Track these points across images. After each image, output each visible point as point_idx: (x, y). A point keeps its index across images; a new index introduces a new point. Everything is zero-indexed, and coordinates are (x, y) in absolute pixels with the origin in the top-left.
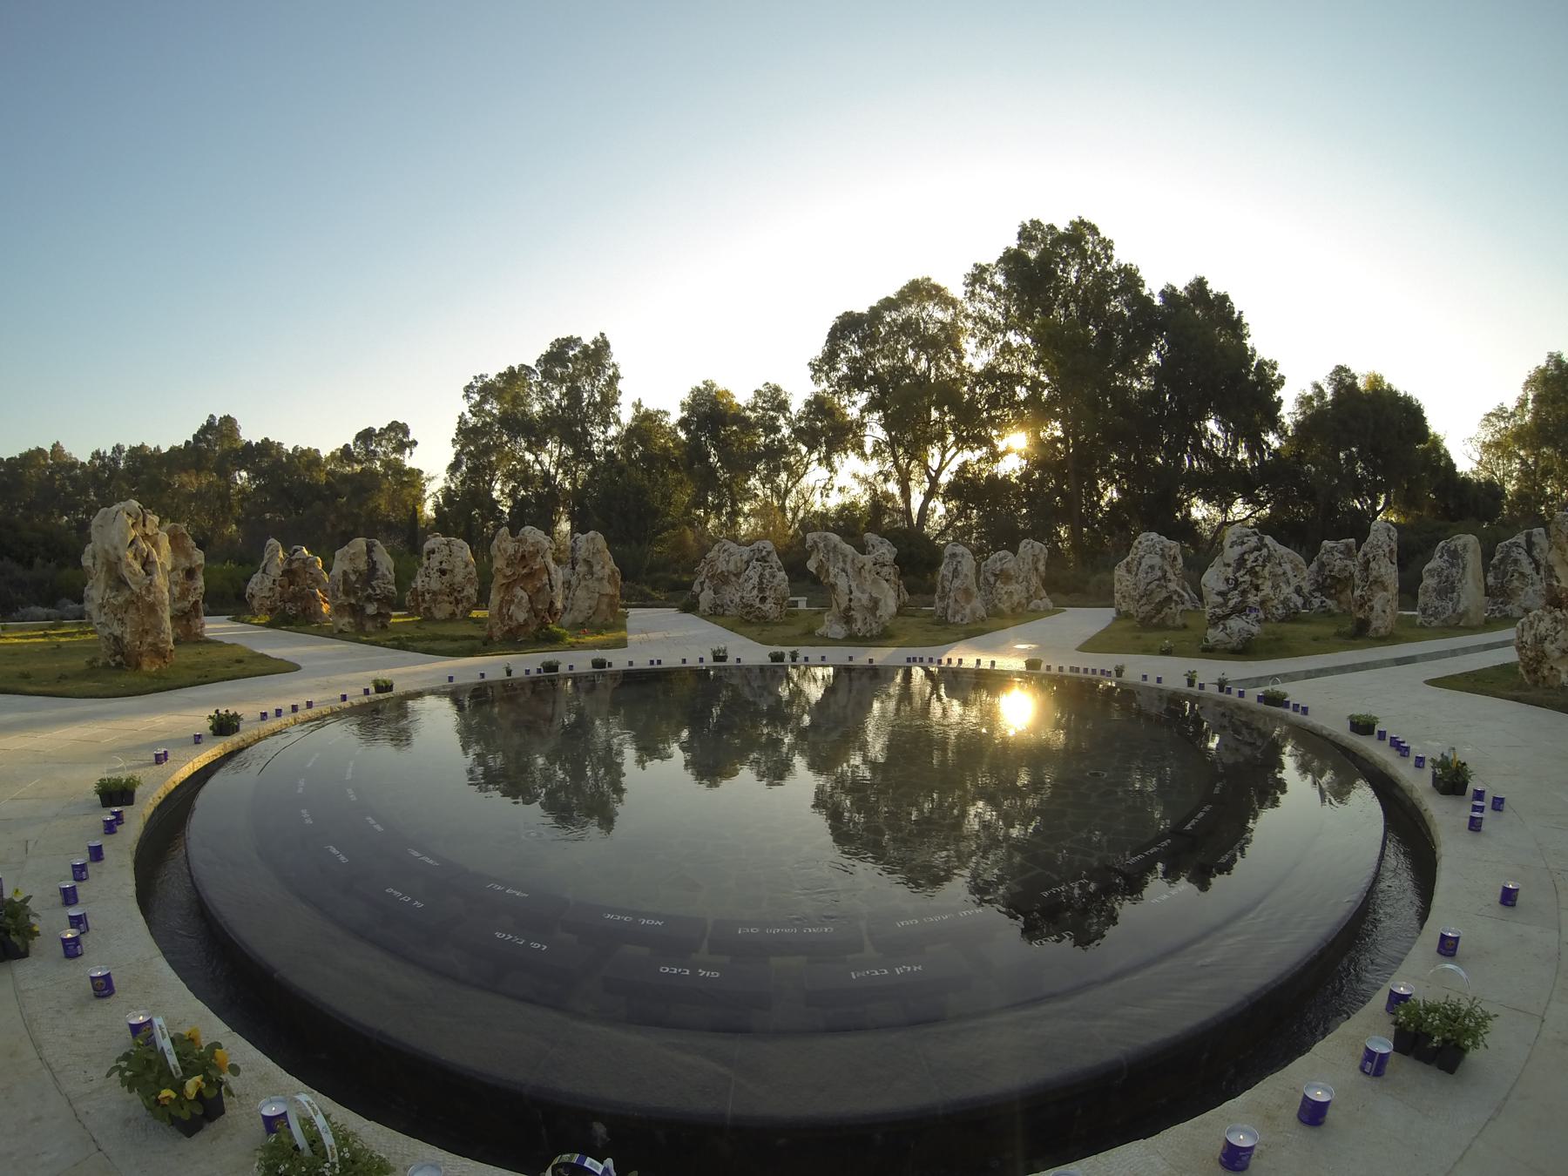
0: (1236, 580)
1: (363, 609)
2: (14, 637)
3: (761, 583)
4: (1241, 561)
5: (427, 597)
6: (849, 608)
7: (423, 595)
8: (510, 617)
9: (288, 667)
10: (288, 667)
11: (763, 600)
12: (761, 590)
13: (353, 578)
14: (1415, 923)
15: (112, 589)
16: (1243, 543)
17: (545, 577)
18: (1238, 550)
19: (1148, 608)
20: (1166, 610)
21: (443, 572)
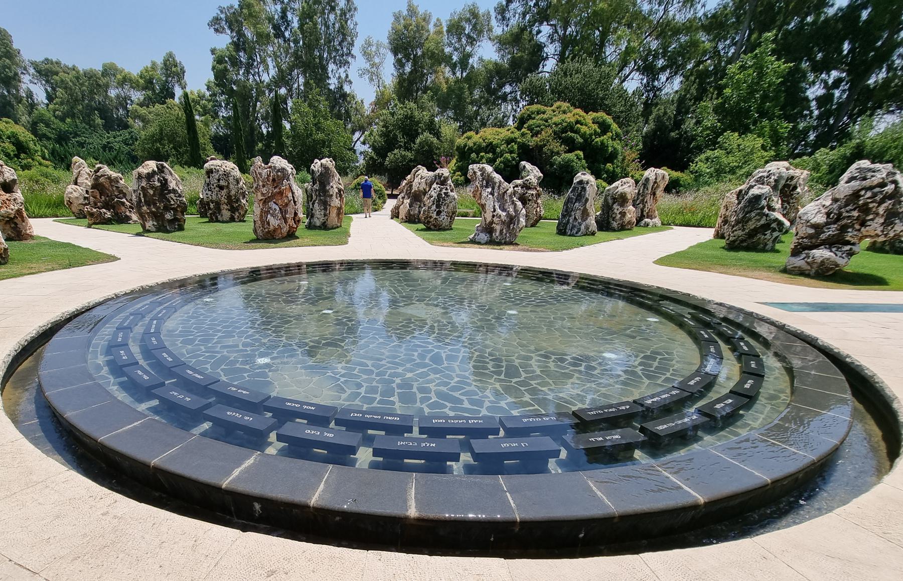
0: (840, 214)
1: (163, 216)
2: (2, 270)
3: (438, 201)
4: (856, 195)
5: (212, 206)
6: (492, 222)
7: (209, 205)
8: (268, 223)
9: (667, 261)
10: (667, 261)
11: (439, 213)
12: (438, 206)
13: (151, 192)
14: (846, 451)
15: (60, 132)
16: (865, 179)
17: (290, 195)
18: (855, 184)
19: (740, 233)
20: (759, 236)
21: (221, 188)
